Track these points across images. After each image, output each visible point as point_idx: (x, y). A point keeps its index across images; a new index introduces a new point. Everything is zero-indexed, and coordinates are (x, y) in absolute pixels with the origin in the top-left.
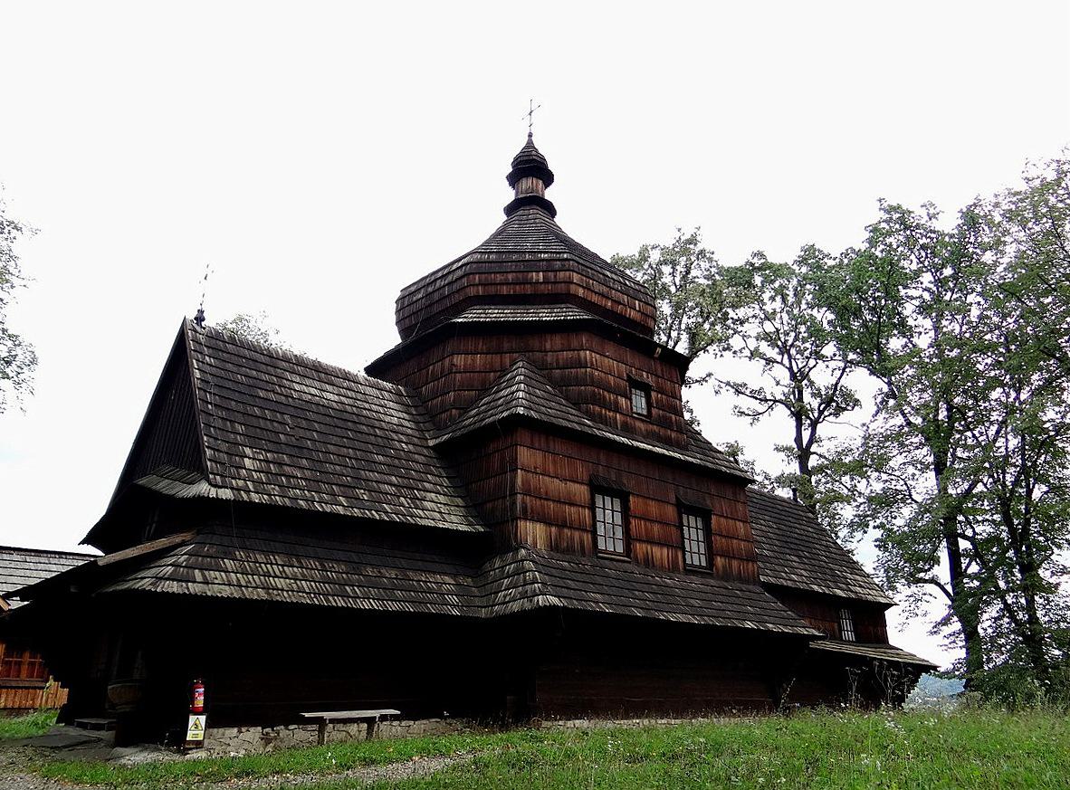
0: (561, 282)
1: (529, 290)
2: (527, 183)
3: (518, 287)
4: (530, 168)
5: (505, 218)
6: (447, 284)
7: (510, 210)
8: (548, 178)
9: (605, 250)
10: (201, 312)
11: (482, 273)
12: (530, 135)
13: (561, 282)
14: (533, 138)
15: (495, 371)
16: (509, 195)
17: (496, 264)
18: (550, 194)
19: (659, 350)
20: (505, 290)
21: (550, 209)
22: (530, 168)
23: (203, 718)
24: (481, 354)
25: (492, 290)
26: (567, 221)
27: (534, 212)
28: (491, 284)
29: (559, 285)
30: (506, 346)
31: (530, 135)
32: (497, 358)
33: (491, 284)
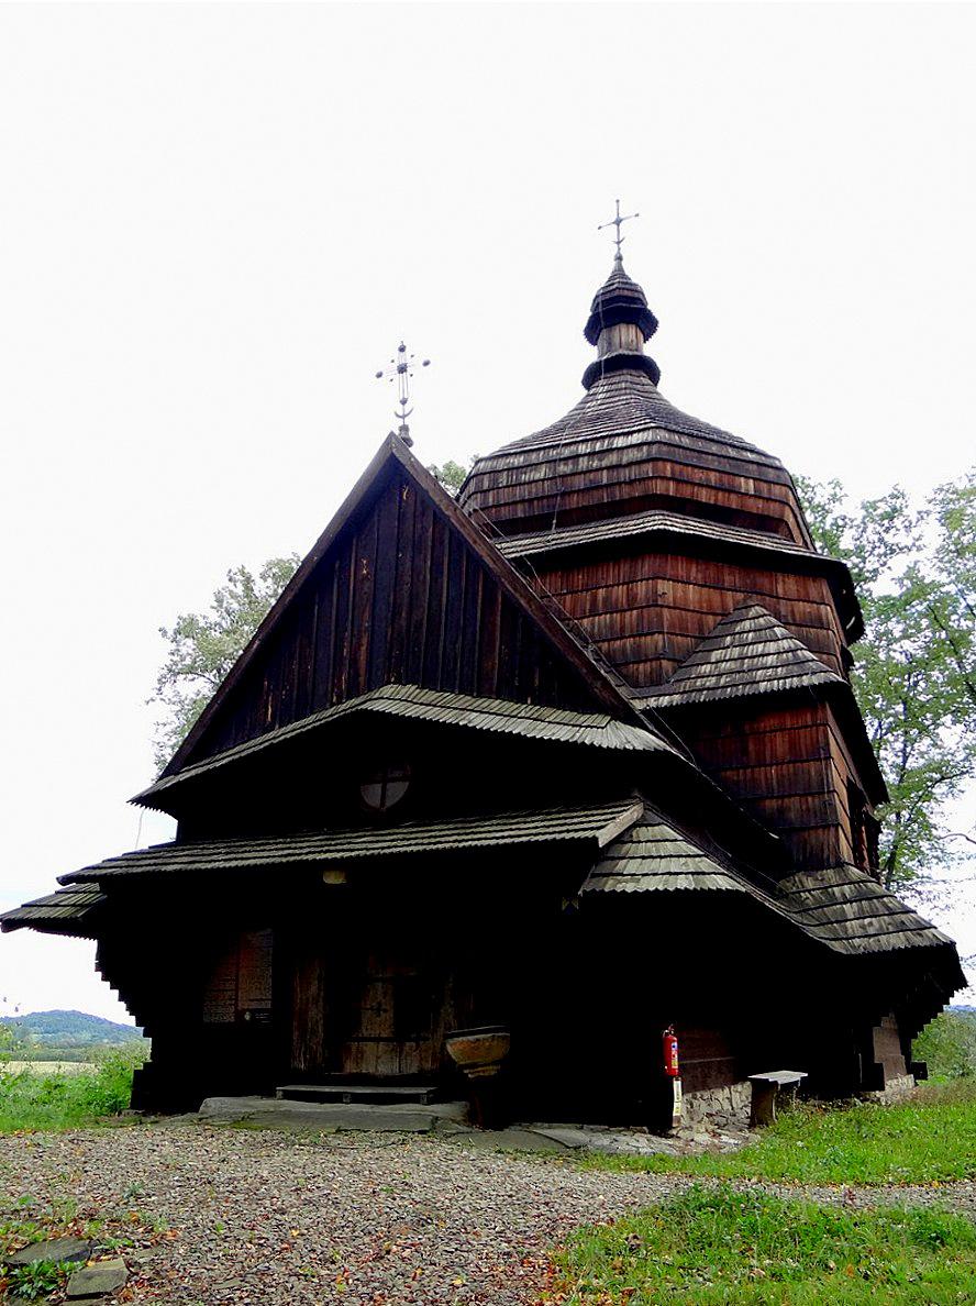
0: (776, 501)
1: (734, 502)
2: (626, 334)
3: (720, 494)
4: (620, 309)
5: (585, 392)
6: (608, 468)
7: (592, 377)
8: (648, 325)
9: (426, 464)
10: (404, 428)
11: (677, 462)
12: (619, 258)
13: (776, 501)
14: (623, 263)
15: (714, 614)
16: (591, 354)
17: (715, 458)
18: (649, 349)
19: (529, 702)
20: (704, 496)
21: (649, 369)
22: (620, 309)
23: (679, 1082)
24: (695, 584)
25: (687, 491)
26: (675, 391)
27: (625, 378)
28: (687, 482)
29: (772, 505)
30: (728, 579)
31: (619, 258)
32: (715, 595)
33: (687, 482)
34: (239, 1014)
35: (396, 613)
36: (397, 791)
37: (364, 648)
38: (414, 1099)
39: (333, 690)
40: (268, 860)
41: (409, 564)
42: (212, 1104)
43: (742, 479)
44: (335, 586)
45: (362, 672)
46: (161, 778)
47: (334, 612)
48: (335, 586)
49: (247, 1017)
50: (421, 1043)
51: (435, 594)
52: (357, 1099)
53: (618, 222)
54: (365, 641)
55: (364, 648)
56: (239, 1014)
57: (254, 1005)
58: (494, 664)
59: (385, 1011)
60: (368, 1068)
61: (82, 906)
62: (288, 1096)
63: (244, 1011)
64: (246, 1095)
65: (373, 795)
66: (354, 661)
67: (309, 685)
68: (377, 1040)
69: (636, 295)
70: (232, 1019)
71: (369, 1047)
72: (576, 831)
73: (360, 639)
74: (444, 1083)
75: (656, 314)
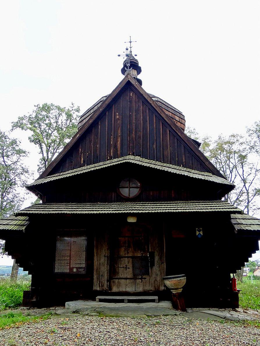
4: (131, 65)
8: (139, 70)
34: (71, 269)
35: (130, 132)
36: (135, 192)
37: (119, 142)
38: (153, 301)
39: (108, 155)
40: (58, 212)
41: (134, 117)
42: (71, 305)
43: (176, 116)
44: (107, 120)
45: (119, 149)
46: (38, 179)
47: (107, 128)
48: (107, 120)
49: (75, 270)
50: (143, 280)
51: (145, 128)
52: (130, 301)
53: (130, 42)
54: (119, 140)
55: (119, 142)
56: (71, 269)
57: (77, 266)
58: (168, 152)
59: (129, 268)
60: (123, 289)
61: (23, 225)
62: (101, 300)
63: (73, 268)
64: (76, 300)
65: (125, 192)
66: (115, 146)
67: (98, 152)
68: (126, 279)
69: (137, 62)
70: (68, 271)
71: (122, 281)
72: (193, 209)
73: (117, 139)
74: (164, 295)
75: (142, 70)
